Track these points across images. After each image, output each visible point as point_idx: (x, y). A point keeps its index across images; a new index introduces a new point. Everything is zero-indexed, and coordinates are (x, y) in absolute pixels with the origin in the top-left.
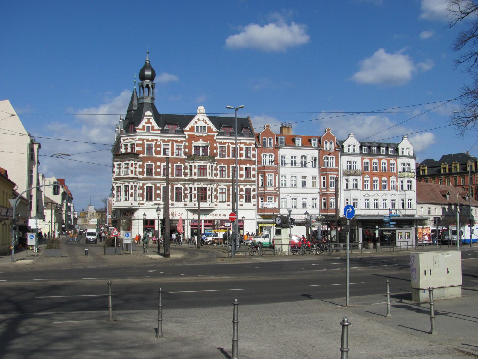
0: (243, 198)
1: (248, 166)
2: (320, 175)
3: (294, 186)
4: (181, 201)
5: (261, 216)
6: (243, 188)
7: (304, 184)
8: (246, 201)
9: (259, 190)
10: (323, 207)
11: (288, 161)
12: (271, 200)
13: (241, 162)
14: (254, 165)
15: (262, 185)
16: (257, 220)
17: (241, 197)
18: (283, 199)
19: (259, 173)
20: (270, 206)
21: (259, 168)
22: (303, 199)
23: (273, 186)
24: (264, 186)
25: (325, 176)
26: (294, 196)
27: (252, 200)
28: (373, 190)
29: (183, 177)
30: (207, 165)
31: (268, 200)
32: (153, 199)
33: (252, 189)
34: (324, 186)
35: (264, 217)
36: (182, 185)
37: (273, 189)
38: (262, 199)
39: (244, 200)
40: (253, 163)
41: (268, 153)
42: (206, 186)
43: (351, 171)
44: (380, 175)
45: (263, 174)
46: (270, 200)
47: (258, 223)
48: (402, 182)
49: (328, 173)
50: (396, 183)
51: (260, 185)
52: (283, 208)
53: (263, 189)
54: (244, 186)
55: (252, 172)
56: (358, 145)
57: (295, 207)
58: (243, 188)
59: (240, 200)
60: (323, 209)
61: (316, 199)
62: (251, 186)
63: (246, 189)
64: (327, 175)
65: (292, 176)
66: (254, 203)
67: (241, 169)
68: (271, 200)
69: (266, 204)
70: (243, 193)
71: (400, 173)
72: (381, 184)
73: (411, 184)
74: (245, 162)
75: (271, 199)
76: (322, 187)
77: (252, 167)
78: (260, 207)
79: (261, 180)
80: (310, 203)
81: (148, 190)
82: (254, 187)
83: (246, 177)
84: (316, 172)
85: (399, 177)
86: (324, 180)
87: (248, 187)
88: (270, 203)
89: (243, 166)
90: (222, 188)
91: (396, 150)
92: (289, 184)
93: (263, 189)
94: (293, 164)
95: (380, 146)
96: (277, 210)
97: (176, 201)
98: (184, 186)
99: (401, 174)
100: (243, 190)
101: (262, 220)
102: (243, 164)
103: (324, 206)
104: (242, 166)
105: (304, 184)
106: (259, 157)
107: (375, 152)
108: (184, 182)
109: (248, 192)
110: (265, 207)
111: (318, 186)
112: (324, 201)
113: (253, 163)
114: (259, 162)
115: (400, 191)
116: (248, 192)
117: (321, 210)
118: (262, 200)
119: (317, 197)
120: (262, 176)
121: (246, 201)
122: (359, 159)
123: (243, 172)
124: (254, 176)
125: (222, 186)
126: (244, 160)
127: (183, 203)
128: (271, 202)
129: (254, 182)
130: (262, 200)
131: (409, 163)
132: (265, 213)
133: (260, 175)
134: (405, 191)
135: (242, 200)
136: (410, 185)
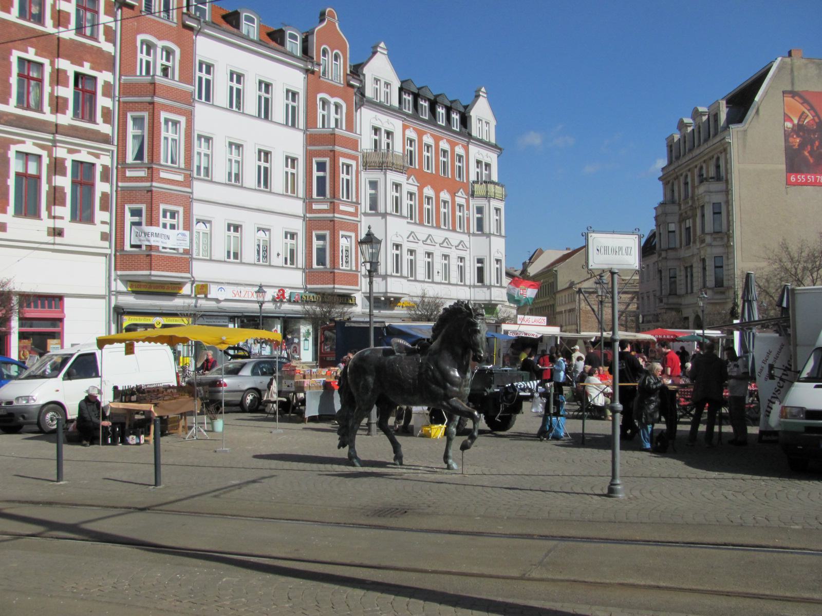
0: (63, 204)
1: (86, 69)
2: (309, 156)
3: (236, 179)
4: (36, 215)
5: (127, 281)
6: (64, 160)
7: (264, 177)
8: (74, 218)
9: (122, 177)
10: (315, 266)
11: (221, 88)
12: (174, 222)
13: (58, 48)
14: (109, 70)
15: (139, 156)
16: (113, 298)
17: (56, 196)
18: (201, 225)
19: (125, 108)
20: (169, 244)
21: (127, 89)
22: (259, 229)
23: (182, 166)
24: (152, 160)
25: (327, 160)
26: (236, 216)
27: (100, 216)
28: (426, 224)
29: (47, 115)
30: (95, 78)
31: (162, 220)
32: (44, 213)
33: (99, 170)
34: (321, 191)
35: (140, 288)
36: (42, 147)
37: (180, 178)
38: (136, 213)
39: (64, 211)
40: (104, 61)
41: (160, 39)
42: (91, 159)
43: (380, 162)
44: (438, 183)
45: (146, 115)
46: (169, 221)
47: (119, 312)
48: (480, 210)
49: (337, 148)
50: (466, 212)
51: (130, 159)
52: (201, 257)
53: (142, 173)
54: (71, 151)
55: (102, 102)
56: (396, 84)
57: (236, 256)
58: (64, 160)
59: (49, 209)
60: (317, 271)
61: (293, 236)
62: (97, 156)
63: (76, 163)
64: (334, 156)
65: (231, 144)
66: (106, 229)
67: (58, 77)
68: (174, 222)
69: (157, 235)
70: (64, 182)
71: (476, 186)
72: (423, 206)
73: (267, 165)
74: (76, 53)
75: (173, 215)
76: (315, 195)
77: (104, 77)
78: (127, 247)
79: (135, 137)
80: (279, 246)
81: (77, 177)
82: (105, 160)
83: (76, 115)
84: (292, 142)
85: (473, 195)
86: (321, 174)
87: (84, 156)
88: (168, 231)
89: (67, 66)
90: (27, 154)
91: (465, 121)
92: (220, 172)
93: (142, 173)
94: (236, 99)
95: (438, 99)
96: (183, 261)
97: (18, 213)
98: (49, 150)
99: (479, 189)
100: (65, 168)
101: (130, 301)
102: (67, 57)
103: (321, 261)
104: (64, 64)
105: (264, 177)
106: (129, 50)
107: (425, 116)
108: (50, 137)
109: (84, 175)
110: (150, 247)
111: (301, 192)
112: (321, 242)
113: (104, 61)
114: (128, 64)
115: (474, 234)
116: (84, 175)
117: (310, 275)
118: (136, 219)
119: (298, 226)
120: (138, 121)
121: (74, 218)
122: (395, 124)
123: (67, 92)
124: (107, 115)
125: (29, 147)
126: (71, 39)
127: (46, 223)
128: (173, 227)
129: (106, 139)
130: (136, 219)
131: (390, 129)
132: (153, 273)
133: (129, 115)
134: (489, 235)
135: (58, 210)
136: (266, 169)
